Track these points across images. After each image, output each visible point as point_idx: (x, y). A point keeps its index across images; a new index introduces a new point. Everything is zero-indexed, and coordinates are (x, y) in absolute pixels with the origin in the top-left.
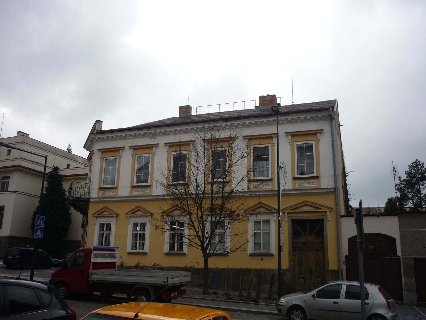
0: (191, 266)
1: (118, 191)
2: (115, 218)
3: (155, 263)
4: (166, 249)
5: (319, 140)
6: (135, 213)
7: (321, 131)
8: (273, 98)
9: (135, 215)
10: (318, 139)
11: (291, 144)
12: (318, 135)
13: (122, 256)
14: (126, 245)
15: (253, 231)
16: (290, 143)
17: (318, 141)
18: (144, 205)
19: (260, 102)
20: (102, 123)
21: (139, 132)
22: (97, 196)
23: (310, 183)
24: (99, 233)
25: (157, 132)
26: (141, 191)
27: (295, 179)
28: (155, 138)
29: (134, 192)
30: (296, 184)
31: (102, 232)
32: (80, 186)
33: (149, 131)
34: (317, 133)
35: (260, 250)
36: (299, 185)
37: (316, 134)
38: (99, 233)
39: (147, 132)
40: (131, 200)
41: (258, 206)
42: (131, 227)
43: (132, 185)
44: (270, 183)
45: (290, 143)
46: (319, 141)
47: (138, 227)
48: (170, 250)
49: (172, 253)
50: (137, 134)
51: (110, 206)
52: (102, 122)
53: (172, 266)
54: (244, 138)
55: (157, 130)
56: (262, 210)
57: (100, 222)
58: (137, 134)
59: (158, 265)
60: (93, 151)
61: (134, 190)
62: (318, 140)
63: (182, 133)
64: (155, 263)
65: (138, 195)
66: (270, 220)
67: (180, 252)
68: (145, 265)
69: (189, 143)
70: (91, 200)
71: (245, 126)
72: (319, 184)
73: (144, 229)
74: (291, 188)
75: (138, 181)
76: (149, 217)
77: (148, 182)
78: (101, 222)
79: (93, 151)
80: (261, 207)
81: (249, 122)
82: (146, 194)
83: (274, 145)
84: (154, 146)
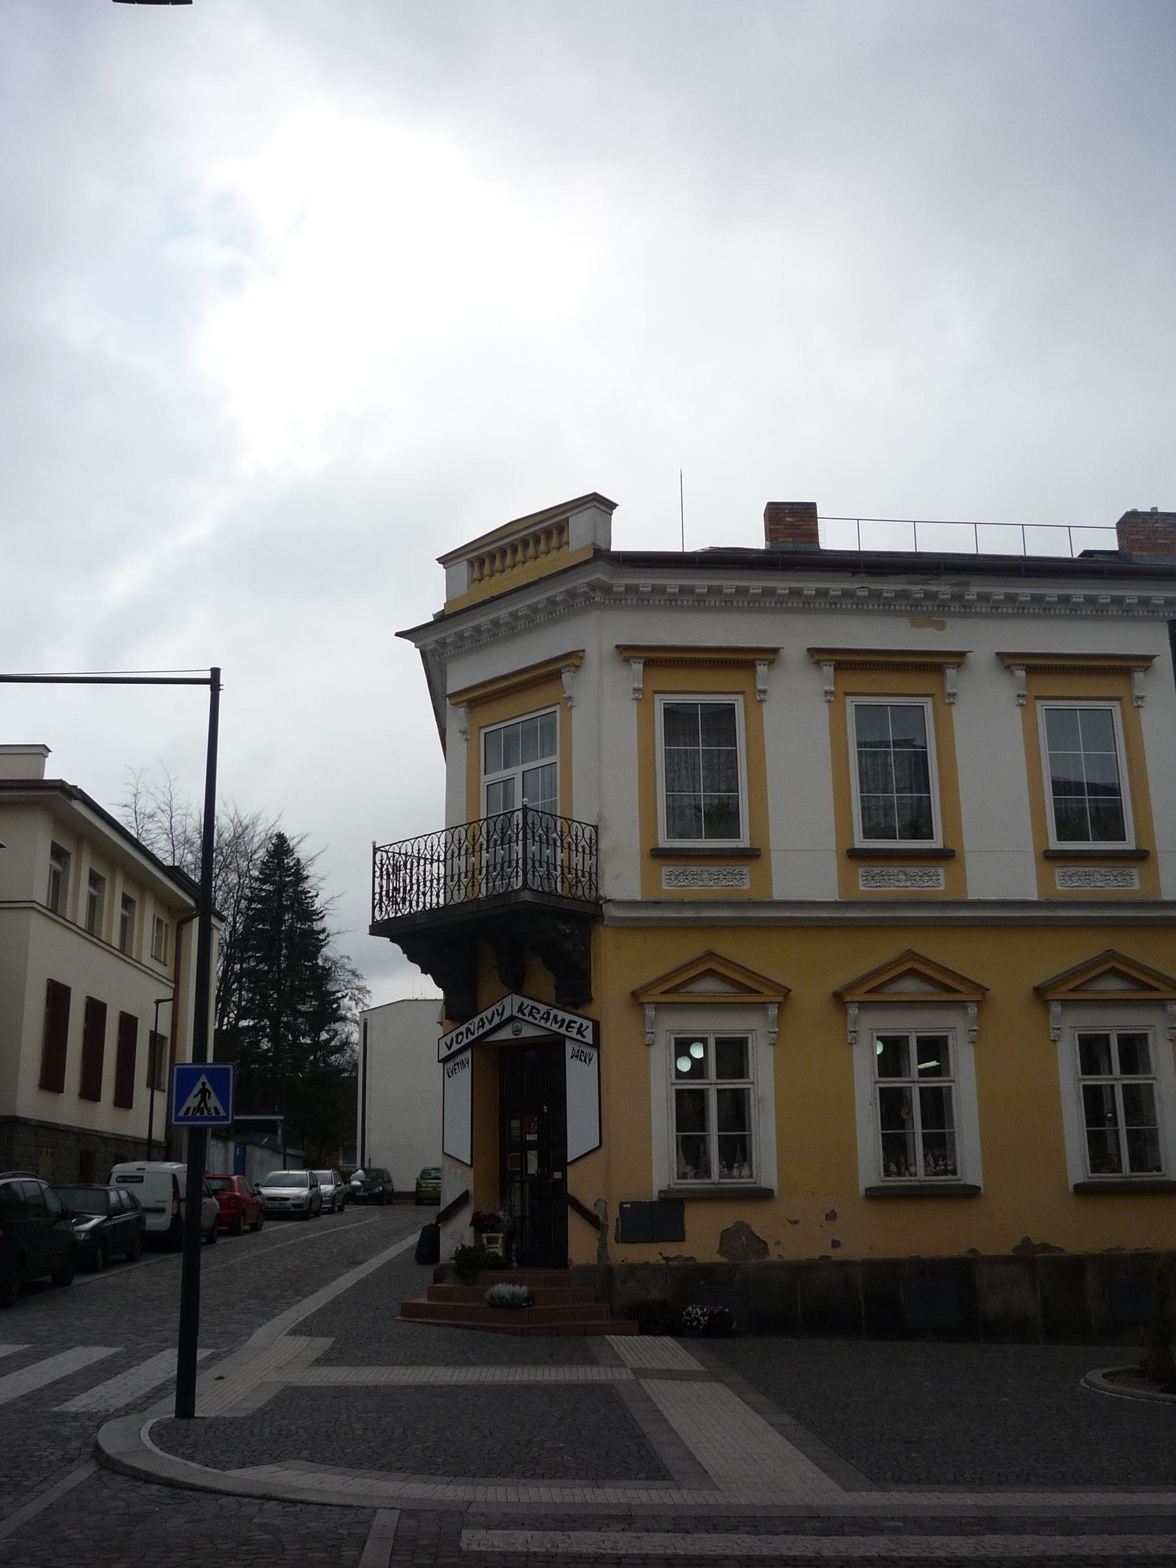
0: (1136, 1249)
1: (1157, 867)
2: (773, 1011)
3: (1027, 1240)
4: (1078, 1168)
5: (953, 695)
6: (886, 990)
7: (770, 657)
8: (1156, 508)
9: (684, 999)
10: (760, 687)
11: (832, 699)
12: (761, 669)
13: (833, 1212)
14: (850, 1149)
15: (876, 1082)
16: (637, 695)
17: (758, 699)
18: (730, 947)
19: (812, 511)
20: (611, 514)
21: (873, 587)
22: (642, 894)
23: (1112, 878)
24: (679, 1093)
25: (967, 597)
26: (903, 877)
27: (1051, 857)
28: (941, 626)
29: (861, 883)
30: (1057, 882)
31: (1131, 1080)
32: (495, 837)
33: (926, 587)
34: (945, 665)
35: (707, 1173)
36: (872, 883)
37: (750, 666)
38: (677, 1091)
39: (914, 588)
40: (732, 918)
41: (700, 969)
42: (1068, 1057)
43: (850, 847)
44: (745, 870)
45: (637, 695)
46: (1139, 703)
47: (879, 1056)
48: (1095, 1169)
49: (1108, 1184)
50: (858, 593)
51: (730, 947)
52: (612, 506)
53: (1119, 1249)
54: (817, 657)
55: (967, 584)
56: (709, 986)
57: (672, 1032)
58: (858, 593)
59: (1045, 1247)
60: (580, 654)
61: (861, 871)
62: (760, 691)
63: (1086, 614)
64: (1027, 1240)
65: (889, 898)
66: (750, 1036)
67: (1147, 1179)
68: (973, 1251)
69: (1131, 664)
70: (610, 911)
71: (823, 605)
72: (766, 880)
73: (740, 1071)
74: (1034, 897)
75: (678, 823)
76: (973, 1010)
77: (929, 836)
78: (683, 1032)
79: (580, 654)
80: (710, 973)
81: (1112, 596)
82: (930, 891)
83: (762, 701)
84: (945, 660)
